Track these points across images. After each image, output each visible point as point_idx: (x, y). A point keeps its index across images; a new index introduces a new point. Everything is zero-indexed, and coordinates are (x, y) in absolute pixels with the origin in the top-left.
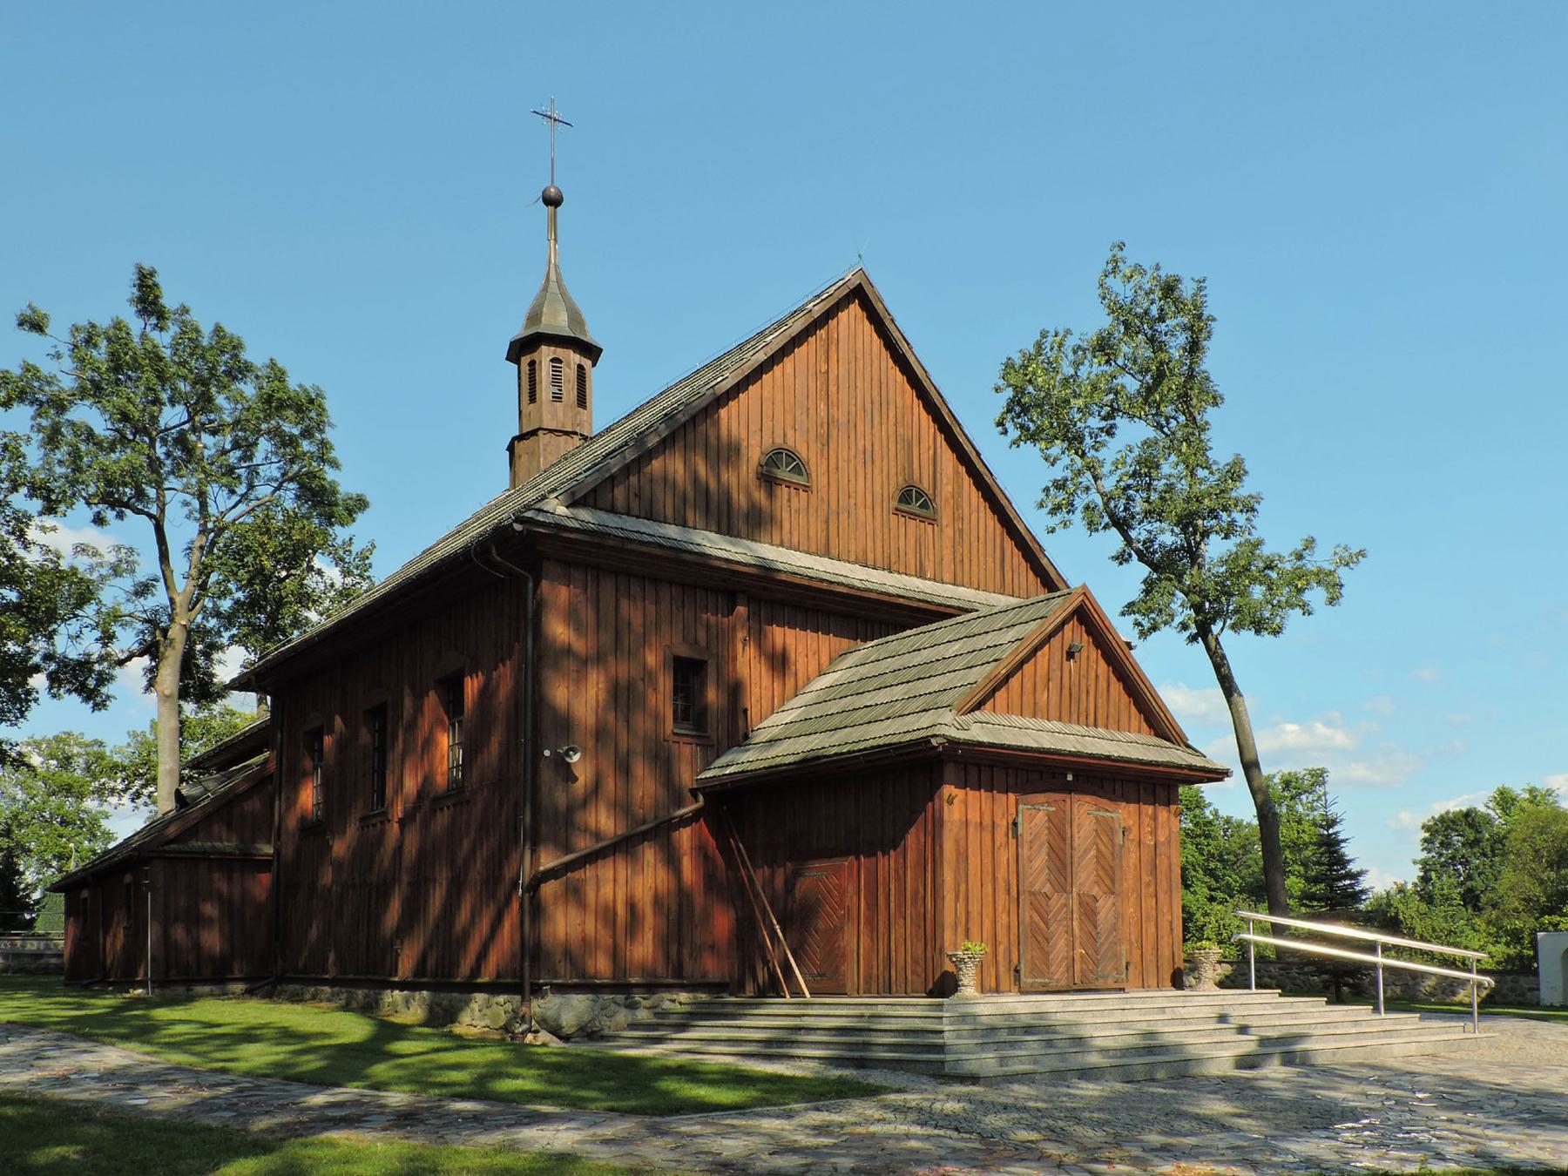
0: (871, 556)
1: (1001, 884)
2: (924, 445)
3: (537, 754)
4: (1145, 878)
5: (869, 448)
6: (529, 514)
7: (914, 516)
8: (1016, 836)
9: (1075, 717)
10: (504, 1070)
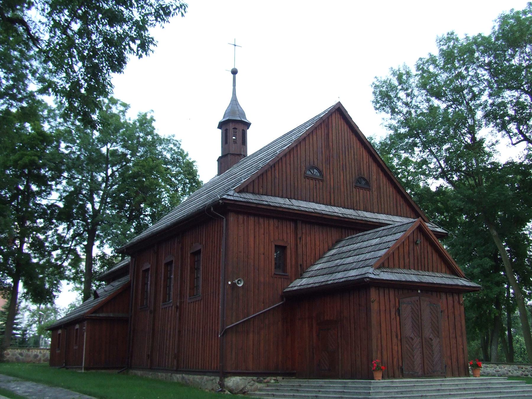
0: (346, 204)
1: (394, 334)
2: (365, 162)
3: (226, 283)
4: (451, 331)
5: (344, 164)
6: (224, 197)
7: (362, 188)
8: (399, 315)
9: (420, 268)
10: (178, 310)
